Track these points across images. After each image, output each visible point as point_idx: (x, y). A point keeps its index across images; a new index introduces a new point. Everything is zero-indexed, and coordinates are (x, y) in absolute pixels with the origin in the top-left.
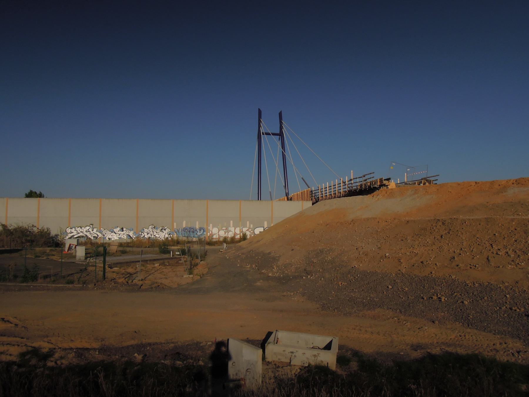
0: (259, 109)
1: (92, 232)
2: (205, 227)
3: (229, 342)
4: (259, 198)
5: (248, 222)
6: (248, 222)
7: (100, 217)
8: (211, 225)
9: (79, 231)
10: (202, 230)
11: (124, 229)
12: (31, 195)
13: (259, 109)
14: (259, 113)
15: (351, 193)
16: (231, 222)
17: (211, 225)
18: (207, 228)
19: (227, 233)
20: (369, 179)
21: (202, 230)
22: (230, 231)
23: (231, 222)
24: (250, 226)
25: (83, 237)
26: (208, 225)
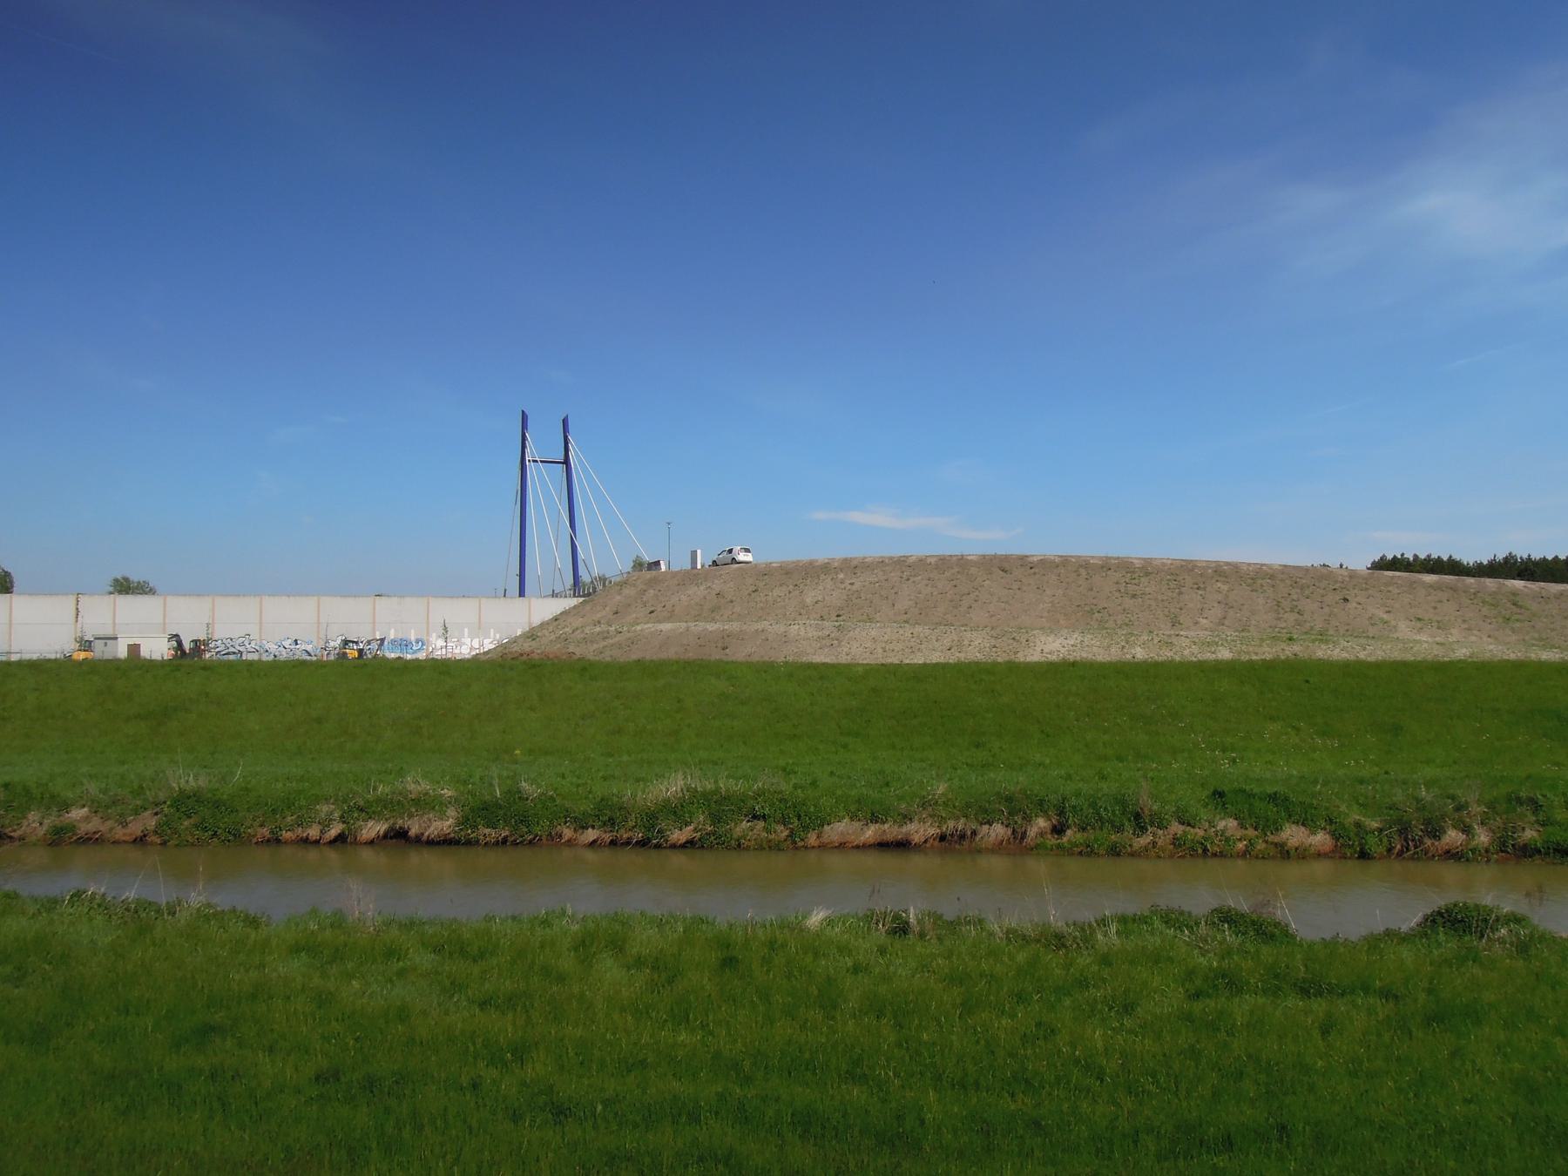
0: (523, 411)
1: (248, 646)
2: (425, 638)
3: (563, 453)
4: (522, 594)
5: (492, 630)
6: (492, 630)
7: (261, 623)
8: (434, 635)
9: (228, 645)
10: (420, 643)
11: (299, 642)
12: (124, 587)
13: (523, 411)
14: (523, 419)
15: (77, 621)
16: (466, 630)
17: (434, 635)
18: (428, 640)
19: (459, 648)
20: (318, 632)
21: (420, 643)
22: (464, 644)
23: (466, 630)
24: (495, 635)
25: (234, 653)
26: (428, 634)
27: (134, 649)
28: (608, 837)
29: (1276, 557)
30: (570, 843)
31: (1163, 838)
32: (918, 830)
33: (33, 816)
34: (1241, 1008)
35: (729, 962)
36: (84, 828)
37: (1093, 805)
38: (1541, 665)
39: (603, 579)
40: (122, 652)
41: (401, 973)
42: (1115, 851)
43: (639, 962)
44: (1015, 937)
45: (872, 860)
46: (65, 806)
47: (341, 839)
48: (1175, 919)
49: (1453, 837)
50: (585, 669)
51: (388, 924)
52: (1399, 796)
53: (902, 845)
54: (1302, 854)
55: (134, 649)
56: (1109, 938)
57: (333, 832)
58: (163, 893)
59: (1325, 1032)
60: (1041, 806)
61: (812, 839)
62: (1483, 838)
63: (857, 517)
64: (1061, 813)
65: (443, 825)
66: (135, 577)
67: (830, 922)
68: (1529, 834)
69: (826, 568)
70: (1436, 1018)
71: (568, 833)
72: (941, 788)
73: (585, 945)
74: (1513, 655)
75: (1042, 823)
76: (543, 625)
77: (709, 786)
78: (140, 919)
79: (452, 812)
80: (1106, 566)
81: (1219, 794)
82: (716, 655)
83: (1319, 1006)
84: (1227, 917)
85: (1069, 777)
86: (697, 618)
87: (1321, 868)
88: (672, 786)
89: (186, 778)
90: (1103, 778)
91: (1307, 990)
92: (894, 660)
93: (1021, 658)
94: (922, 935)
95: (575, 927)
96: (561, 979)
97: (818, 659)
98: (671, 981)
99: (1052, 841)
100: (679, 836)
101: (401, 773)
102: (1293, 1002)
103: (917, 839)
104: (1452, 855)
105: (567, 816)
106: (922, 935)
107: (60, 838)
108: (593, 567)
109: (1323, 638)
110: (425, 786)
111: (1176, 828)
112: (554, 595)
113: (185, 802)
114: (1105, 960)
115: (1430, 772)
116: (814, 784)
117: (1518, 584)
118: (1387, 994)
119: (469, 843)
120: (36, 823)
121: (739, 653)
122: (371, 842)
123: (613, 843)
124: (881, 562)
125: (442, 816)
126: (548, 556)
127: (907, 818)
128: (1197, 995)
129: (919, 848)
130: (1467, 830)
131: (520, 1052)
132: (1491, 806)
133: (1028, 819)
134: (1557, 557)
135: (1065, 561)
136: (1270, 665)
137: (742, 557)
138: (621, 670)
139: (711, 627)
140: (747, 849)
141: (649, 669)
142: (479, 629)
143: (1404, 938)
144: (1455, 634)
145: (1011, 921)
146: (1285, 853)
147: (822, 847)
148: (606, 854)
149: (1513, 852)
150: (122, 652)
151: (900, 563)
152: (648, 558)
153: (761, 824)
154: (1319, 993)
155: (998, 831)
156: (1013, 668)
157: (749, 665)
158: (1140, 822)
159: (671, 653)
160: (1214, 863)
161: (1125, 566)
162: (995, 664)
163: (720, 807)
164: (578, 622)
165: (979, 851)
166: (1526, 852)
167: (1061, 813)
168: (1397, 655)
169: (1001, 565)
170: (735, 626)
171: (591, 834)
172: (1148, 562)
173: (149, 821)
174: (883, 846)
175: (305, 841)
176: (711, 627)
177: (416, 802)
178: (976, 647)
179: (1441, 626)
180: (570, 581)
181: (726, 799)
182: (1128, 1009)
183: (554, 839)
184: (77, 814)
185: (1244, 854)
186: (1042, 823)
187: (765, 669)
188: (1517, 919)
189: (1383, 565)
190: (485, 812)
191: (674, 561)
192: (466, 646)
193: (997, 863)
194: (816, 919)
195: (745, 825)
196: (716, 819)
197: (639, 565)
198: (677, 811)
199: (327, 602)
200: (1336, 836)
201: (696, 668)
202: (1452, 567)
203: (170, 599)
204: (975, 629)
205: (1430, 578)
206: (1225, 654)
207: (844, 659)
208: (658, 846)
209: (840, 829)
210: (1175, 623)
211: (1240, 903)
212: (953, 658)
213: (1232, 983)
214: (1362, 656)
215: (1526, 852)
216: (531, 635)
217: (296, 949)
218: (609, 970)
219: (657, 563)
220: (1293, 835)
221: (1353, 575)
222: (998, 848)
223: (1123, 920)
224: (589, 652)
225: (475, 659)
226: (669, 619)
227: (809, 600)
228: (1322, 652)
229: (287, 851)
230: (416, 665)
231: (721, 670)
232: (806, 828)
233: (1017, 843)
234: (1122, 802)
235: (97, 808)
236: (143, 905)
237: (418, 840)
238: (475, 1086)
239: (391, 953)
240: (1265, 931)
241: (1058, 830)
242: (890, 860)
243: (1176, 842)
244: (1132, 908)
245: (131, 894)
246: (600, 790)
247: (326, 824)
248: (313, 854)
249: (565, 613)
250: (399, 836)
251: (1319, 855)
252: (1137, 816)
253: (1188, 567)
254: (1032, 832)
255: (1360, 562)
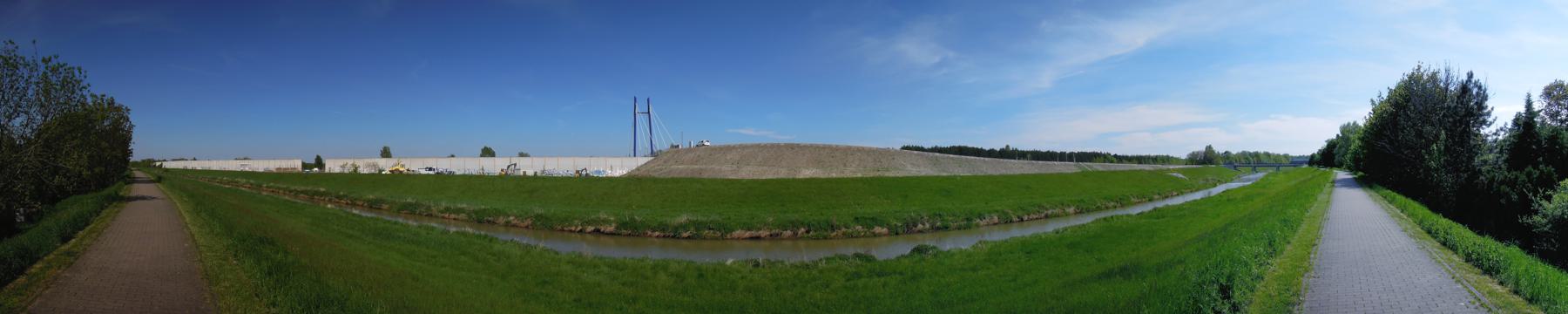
4: (635, 156)
12: (522, 155)
27: (525, 173)
28: (662, 234)
29: (874, 145)
30: (650, 236)
31: (840, 233)
32: (763, 233)
33: (501, 218)
34: (860, 283)
35: (701, 275)
36: (514, 222)
37: (819, 224)
38: (943, 177)
39: (661, 151)
40: (522, 174)
41: (598, 272)
42: (825, 238)
43: (672, 274)
44: (792, 265)
45: (748, 243)
46: (509, 216)
47: (581, 231)
48: (843, 257)
49: (920, 226)
50: (655, 180)
51: (595, 257)
52: (906, 215)
53: (758, 238)
54: (880, 235)
55: (525, 173)
56: (822, 265)
57: (579, 228)
58: (533, 243)
59: (884, 287)
60: (803, 224)
61: (728, 236)
62: (927, 226)
63: (743, 131)
64: (809, 226)
65: (611, 229)
66: (525, 152)
67: (734, 263)
68: (939, 224)
69: (734, 147)
70: (914, 278)
71: (649, 233)
72: (771, 219)
73: (655, 268)
74: (936, 174)
75: (803, 230)
76: (642, 166)
77: (695, 219)
78: (527, 249)
79: (613, 225)
80: (824, 147)
81: (857, 219)
82: (697, 176)
83: (883, 279)
84: (857, 255)
85: (811, 215)
86: (691, 164)
87: (885, 239)
88: (683, 219)
89: (539, 211)
90: (822, 214)
91: (879, 275)
92: (755, 178)
93: (797, 177)
94: (764, 266)
95: (651, 263)
96: (647, 278)
97: (730, 177)
98: (682, 281)
99: (806, 235)
100: (685, 235)
101: (599, 212)
102: (876, 279)
103: (763, 236)
104: (920, 232)
105: (649, 227)
106: (764, 266)
107: (508, 224)
108: (657, 147)
109: (887, 170)
110: (606, 216)
111: (844, 230)
112: (645, 156)
113: (539, 217)
114: (821, 272)
115: (914, 208)
116: (729, 218)
117: (938, 154)
118: (901, 274)
119: (619, 234)
120: (502, 220)
121: (705, 176)
122: (589, 233)
123: (664, 236)
124: (752, 146)
125: (611, 225)
126: (643, 143)
127: (760, 229)
128: (848, 280)
129: (764, 239)
130: (924, 224)
131: (635, 300)
132: (930, 217)
133: (798, 228)
134: (1209, 148)
135: (811, 146)
136: (872, 178)
137: (706, 144)
138: (667, 181)
139: (696, 167)
140: (707, 239)
141: (676, 181)
142: (622, 167)
143: (906, 257)
144: (922, 169)
145: (792, 261)
146: (875, 235)
147: (732, 239)
148: (662, 240)
149: (935, 229)
150: (522, 174)
151: (758, 146)
152: (675, 144)
153: (712, 231)
154: (883, 276)
155: (789, 233)
156: (794, 180)
157: (709, 180)
158: (833, 228)
159: (683, 175)
160: (855, 240)
161: (830, 147)
162: (789, 179)
163: (698, 226)
164: (653, 165)
165: (783, 239)
166: (938, 229)
167: (809, 226)
168: (907, 174)
169: (791, 147)
170: (704, 167)
171: (657, 233)
172: (837, 146)
173: (529, 222)
174: (752, 238)
175: (571, 231)
176: (696, 167)
177: (603, 221)
178: (783, 173)
179: (919, 166)
180: (650, 151)
181: (701, 223)
182: (827, 286)
183: (645, 235)
184: (511, 218)
185: (863, 236)
186: (803, 230)
187: (713, 181)
188: (934, 247)
189: (904, 148)
190: (624, 225)
191: (684, 145)
192: (618, 173)
193: (789, 243)
194: (729, 262)
195: (707, 232)
196: (697, 229)
197: (672, 146)
198: (684, 227)
199: (576, 159)
200: (889, 229)
201: (692, 180)
202: (922, 149)
203: (534, 159)
204: (782, 167)
205: (916, 152)
206: (859, 175)
207: (740, 178)
208: (678, 238)
209: (738, 233)
210: (845, 165)
211: (861, 251)
212: (776, 177)
213: (858, 275)
214: (898, 175)
215: (938, 229)
216: (638, 169)
217: (569, 262)
218: (662, 276)
219: (678, 146)
220: (878, 229)
221: (896, 151)
222: (789, 238)
223: (827, 259)
224: (656, 175)
225: (620, 177)
226: (682, 164)
227: (728, 158)
228: (887, 174)
229: (566, 234)
230: (603, 178)
231: (700, 181)
232: (727, 233)
233: (795, 237)
234: (827, 222)
235: (516, 217)
236: (527, 246)
237: (603, 233)
238: (621, 309)
239: (595, 266)
240: (868, 259)
241: (808, 232)
242: (753, 243)
243: (844, 234)
244: (830, 255)
245: (525, 242)
246: (659, 219)
247: (577, 227)
248: (573, 235)
249: (648, 162)
250: (598, 231)
251: (885, 235)
252: (832, 226)
253: (849, 148)
254: (800, 232)
255: (898, 147)
